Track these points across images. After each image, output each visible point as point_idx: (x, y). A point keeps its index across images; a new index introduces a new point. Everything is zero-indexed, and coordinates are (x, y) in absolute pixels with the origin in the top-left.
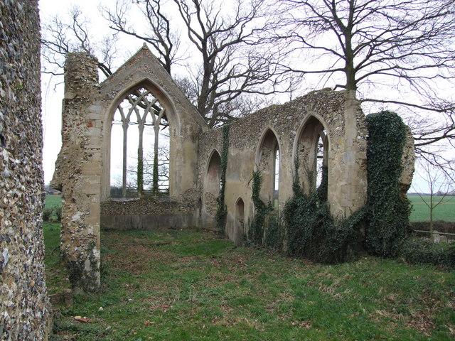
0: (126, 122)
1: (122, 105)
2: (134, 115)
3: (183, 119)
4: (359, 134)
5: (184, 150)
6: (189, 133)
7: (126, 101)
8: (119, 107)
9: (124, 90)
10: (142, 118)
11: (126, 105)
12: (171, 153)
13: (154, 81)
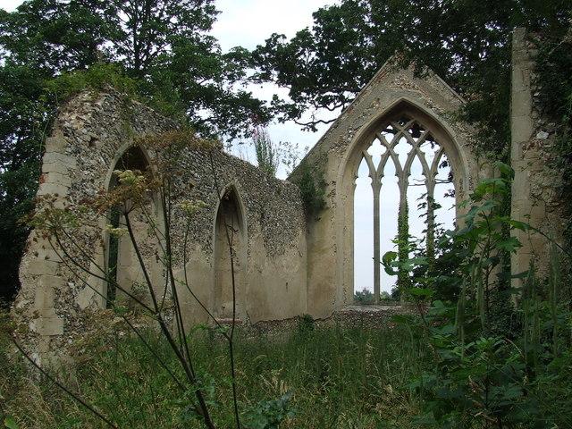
0: (376, 177)
1: (370, 151)
8: (363, 155)
10: (376, 167)
11: (376, 150)
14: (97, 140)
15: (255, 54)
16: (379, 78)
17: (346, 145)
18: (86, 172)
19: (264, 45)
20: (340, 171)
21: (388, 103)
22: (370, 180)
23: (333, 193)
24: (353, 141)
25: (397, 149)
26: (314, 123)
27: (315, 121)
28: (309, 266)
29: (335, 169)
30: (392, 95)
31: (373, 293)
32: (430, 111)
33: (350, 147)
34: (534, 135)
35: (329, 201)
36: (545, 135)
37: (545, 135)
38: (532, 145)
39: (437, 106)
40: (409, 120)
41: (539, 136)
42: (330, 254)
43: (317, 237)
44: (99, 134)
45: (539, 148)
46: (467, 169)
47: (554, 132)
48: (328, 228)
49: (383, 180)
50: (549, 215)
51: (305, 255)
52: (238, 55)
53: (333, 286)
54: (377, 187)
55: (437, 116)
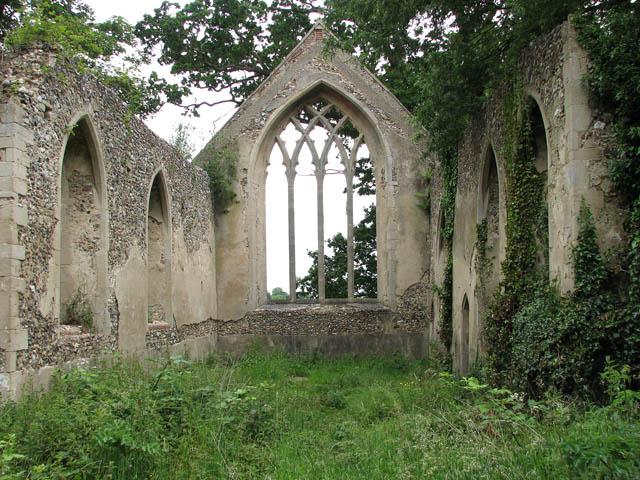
0: (291, 165)
1: (283, 136)
2: (334, 151)
3: (396, 150)
6: (409, 175)
7: (290, 127)
8: (276, 140)
9: (281, 108)
10: (290, 157)
11: (290, 134)
14: (51, 110)
15: (139, 26)
16: (293, 57)
17: (252, 130)
18: (42, 149)
19: (153, 15)
20: (252, 158)
21: (305, 86)
22: (284, 168)
23: (244, 182)
24: (267, 124)
25: (312, 135)
26: (197, 106)
27: (198, 103)
28: (218, 263)
29: (248, 154)
30: (310, 77)
31: (288, 293)
32: (352, 97)
33: (263, 131)
34: (592, 124)
35: (238, 188)
36: (603, 125)
37: (603, 125)
38: (590, 135)
39: (359, 91)
40: (325, 104)
41: (596, 126)
42: (242, 249)
43: (226, 229)
44: (52, 103)
45: (597, 138)
46: (390, 159)
47: (610, 122)
48: (240, 216)
49: (297, 168)
50: (607, 205)
51: (213, 250)
52: (115, 28)
53: (245, 283)
54: (291, 175)
55: (359, 102)
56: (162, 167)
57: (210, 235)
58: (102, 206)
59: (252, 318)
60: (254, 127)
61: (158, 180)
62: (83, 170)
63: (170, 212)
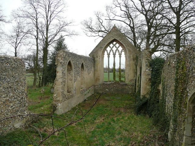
0: (109, 55)
1: (107, 49)
4: (147, 69)
5: (130, 64)
6: (132, 57)
10: (109, 53)
12: (126, 65)
13: (118, 39)
28: (94, 74)
32: (121, 41)
56: (83, 62)
57: (93, 69)
58: (73, 73)
59: (100, 85)
60: (101, 48)
61: (82, 65)
62: (69, 68)
63: (85, 68)
